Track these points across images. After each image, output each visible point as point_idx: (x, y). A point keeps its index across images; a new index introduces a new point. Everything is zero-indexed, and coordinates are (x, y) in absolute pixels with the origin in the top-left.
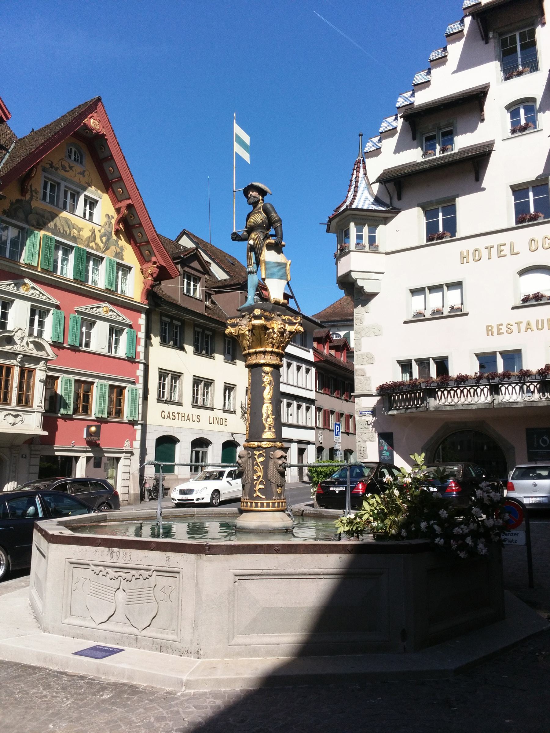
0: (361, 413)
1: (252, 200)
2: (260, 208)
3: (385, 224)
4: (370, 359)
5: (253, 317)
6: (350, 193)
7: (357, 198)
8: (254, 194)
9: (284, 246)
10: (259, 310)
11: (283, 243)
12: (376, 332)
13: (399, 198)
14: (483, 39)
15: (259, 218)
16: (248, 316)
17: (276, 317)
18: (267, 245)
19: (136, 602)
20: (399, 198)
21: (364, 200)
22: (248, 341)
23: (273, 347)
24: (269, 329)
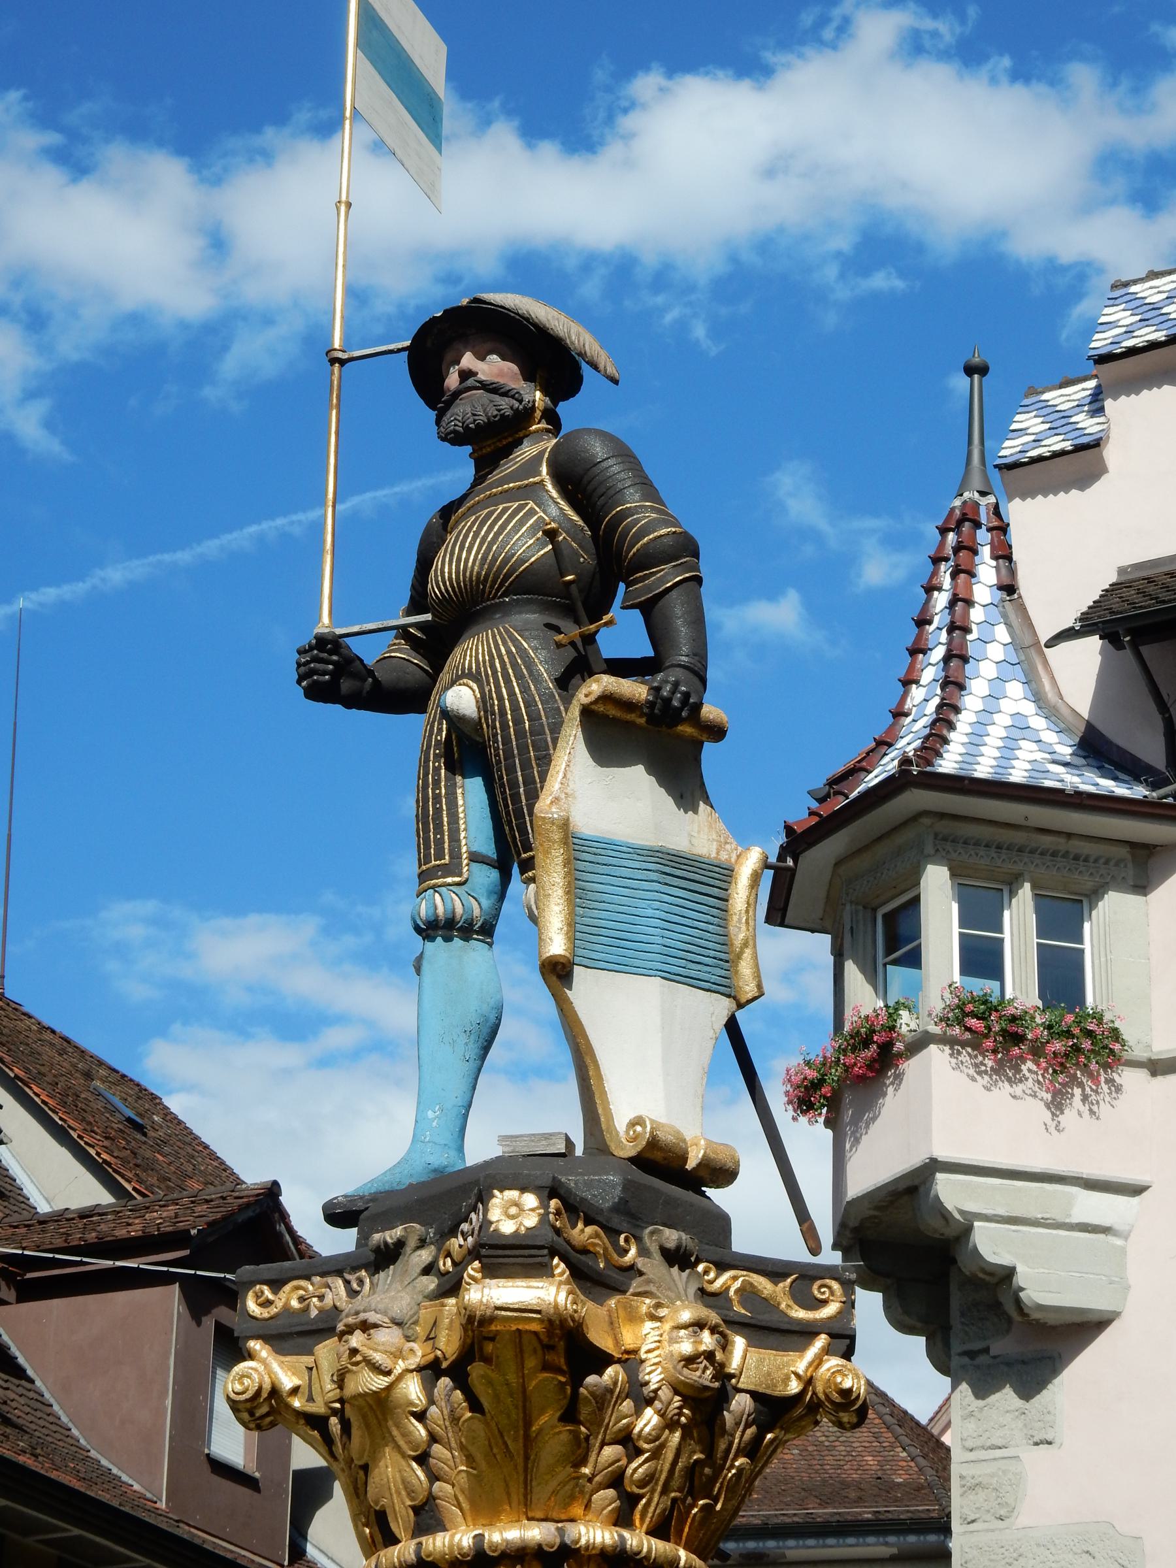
1: (472, 409)
2: (531, 467)
3: (1142, 887)
5: (474, 1254)
6: (917, 694)
7: (964, 722)
8: (493, 367)
9: (717, 732)
10: (530, 1200)
11: (710, 711)
15: (523, 527)
16: (425, 1256)
17: (653, 1266)
18: (588, 714)
21: (1016, 723)
22: (422, 1459)
23: (622, 1519)
24: (602, 1360)
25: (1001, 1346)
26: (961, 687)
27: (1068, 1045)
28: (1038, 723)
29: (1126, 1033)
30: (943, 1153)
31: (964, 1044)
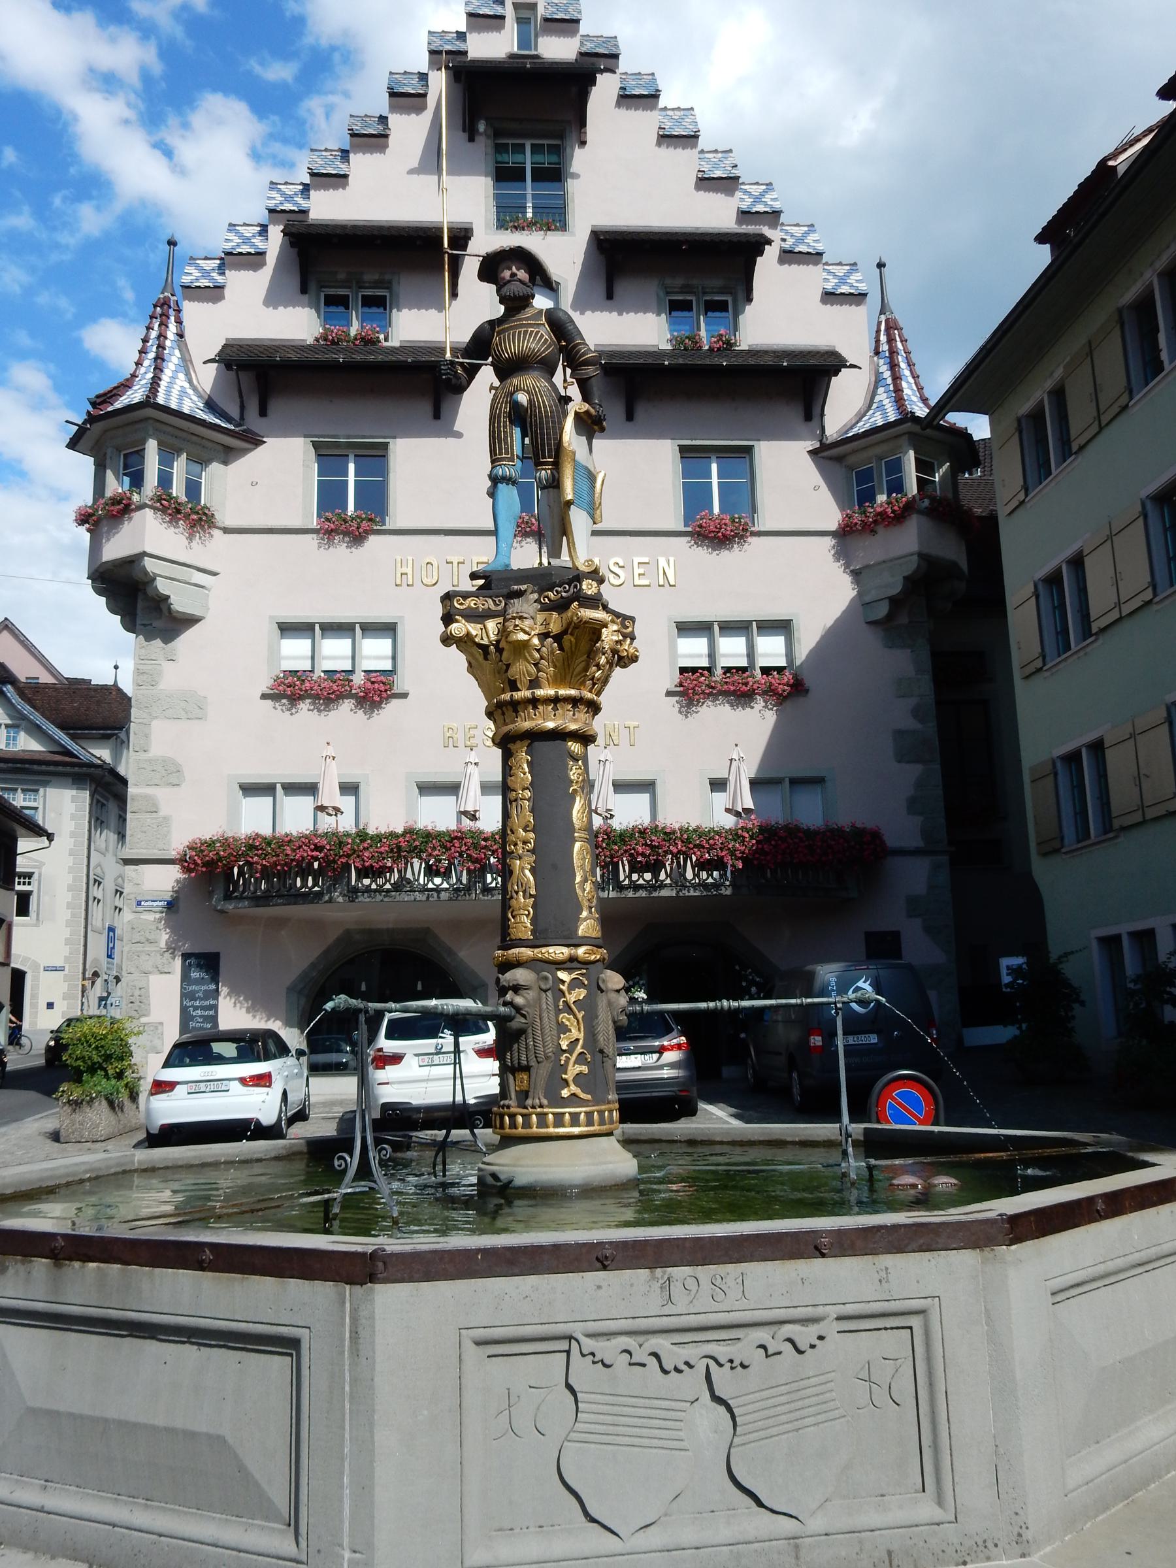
0: (139, 904)
4: (171, 774)
6: (142, 370)
12: (192, 708)
13: (263, 413)
14: (464, 131)
16: (536, 596)
19: (774, 1431)
20: (263, 413)
25: (156, 624)
26: (162, 371)
27: (194, 516)
28: (190, 392)
29: (216, 516)
30: (148, 550)
31: (159, 510)
